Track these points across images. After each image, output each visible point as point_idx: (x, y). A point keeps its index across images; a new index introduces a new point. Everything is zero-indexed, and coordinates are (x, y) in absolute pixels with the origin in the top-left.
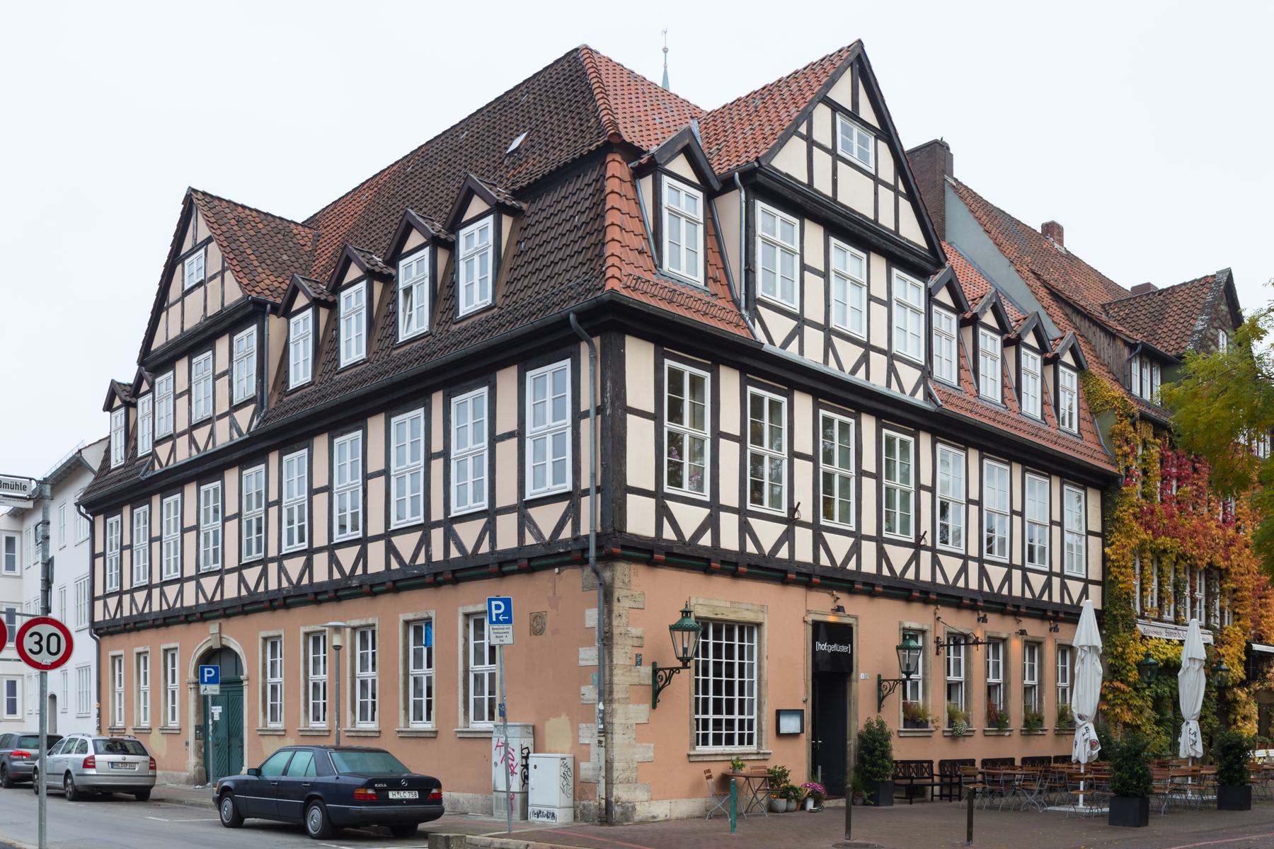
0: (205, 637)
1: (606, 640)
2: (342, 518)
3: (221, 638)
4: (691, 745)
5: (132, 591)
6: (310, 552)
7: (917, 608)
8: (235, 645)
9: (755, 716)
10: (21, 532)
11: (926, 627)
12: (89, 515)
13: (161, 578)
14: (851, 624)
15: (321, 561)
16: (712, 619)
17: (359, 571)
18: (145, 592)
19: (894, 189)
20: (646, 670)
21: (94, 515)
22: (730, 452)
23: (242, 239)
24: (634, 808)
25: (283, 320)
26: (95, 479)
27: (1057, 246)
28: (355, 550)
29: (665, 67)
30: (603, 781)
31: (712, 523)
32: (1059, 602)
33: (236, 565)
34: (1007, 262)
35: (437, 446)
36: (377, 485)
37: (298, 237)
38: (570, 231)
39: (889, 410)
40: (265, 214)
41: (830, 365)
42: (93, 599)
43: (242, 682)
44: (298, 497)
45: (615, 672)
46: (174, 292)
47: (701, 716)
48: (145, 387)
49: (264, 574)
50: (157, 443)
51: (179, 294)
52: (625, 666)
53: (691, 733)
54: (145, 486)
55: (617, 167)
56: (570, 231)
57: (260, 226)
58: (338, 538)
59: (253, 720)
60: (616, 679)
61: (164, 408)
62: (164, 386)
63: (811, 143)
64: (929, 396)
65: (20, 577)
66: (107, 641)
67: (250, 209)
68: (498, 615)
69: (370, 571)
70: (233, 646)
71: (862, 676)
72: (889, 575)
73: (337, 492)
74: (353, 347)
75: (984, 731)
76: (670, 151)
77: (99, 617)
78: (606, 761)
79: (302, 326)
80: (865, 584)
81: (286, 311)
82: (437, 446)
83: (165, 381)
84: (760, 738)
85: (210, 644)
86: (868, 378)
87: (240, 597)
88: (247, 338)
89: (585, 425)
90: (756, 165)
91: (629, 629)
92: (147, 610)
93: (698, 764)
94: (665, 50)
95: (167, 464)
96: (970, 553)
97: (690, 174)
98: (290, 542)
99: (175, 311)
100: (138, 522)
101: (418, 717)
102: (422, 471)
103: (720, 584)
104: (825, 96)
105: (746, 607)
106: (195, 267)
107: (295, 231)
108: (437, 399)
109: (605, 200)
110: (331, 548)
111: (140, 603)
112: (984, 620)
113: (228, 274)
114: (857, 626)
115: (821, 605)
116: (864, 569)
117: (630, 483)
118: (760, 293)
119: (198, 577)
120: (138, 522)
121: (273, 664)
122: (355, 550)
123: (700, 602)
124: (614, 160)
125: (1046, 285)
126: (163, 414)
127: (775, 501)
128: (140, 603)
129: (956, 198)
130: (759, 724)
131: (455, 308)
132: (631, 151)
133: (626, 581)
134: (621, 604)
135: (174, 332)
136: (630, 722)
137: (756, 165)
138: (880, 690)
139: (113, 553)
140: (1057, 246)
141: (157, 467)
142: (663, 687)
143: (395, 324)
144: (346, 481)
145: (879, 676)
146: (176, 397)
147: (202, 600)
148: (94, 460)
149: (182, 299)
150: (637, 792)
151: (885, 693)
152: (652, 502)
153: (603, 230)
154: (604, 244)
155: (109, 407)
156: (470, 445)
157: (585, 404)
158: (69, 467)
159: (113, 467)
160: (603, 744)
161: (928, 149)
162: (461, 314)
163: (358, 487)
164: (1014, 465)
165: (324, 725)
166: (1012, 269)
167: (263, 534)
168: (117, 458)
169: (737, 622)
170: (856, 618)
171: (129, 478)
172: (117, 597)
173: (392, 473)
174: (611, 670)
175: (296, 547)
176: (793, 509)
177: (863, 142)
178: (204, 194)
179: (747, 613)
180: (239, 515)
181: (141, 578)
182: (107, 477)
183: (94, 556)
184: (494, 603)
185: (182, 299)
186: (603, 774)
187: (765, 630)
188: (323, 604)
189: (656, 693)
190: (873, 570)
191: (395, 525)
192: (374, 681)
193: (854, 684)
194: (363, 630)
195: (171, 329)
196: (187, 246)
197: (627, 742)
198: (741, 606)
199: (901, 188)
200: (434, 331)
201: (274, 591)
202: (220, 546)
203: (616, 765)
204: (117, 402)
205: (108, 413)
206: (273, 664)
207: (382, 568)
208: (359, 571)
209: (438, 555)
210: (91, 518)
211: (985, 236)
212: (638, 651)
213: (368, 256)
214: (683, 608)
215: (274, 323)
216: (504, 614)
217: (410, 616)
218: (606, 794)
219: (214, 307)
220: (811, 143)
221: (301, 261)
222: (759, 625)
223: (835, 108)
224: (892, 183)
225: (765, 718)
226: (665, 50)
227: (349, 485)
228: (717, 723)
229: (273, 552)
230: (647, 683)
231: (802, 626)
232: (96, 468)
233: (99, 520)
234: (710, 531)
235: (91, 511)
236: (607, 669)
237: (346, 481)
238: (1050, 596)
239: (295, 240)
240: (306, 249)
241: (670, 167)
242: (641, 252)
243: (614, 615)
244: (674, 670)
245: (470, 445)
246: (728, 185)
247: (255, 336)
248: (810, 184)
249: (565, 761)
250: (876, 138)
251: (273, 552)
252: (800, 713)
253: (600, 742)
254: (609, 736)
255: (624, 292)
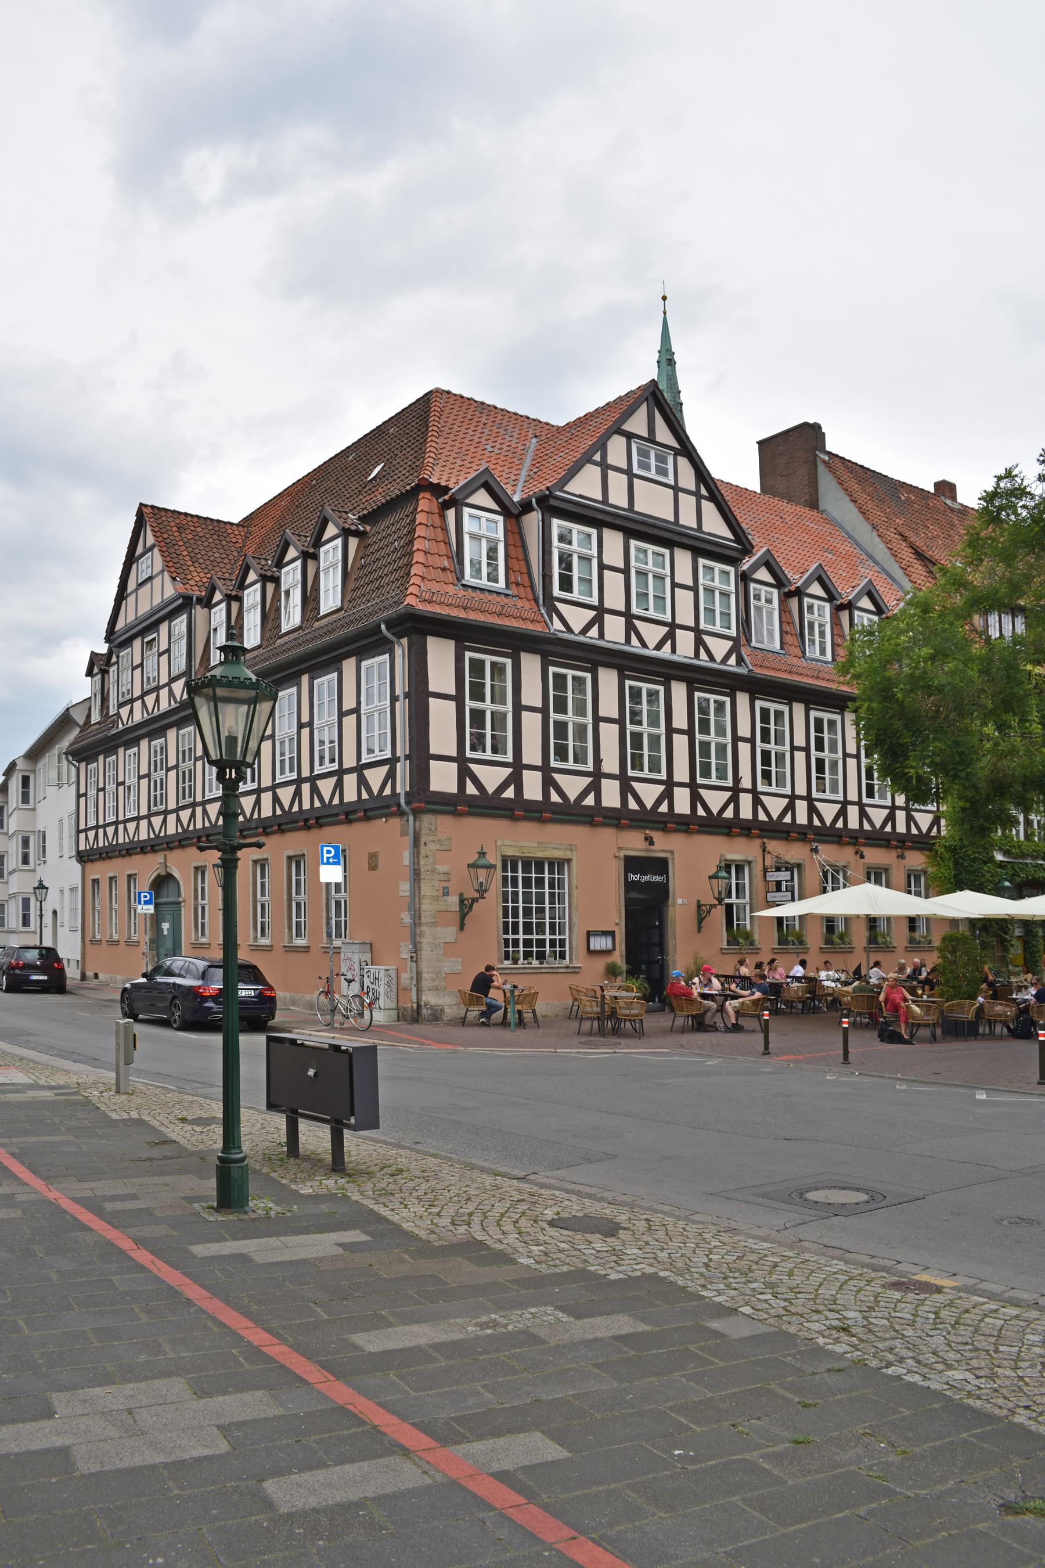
0: (148, 867)
1: (416, 875)
2: (322, 752)
3: (166, 866)
4: (499, 960)
5: (105, 826)
6: (340, 773)
7: (741, 842)
8: (176, 874)
9: (567, 936)
10: (34, 771)
11: (750, 858)
12: (75, 762)
13: (86, 825)
14: (667, 858)
15: (350, 781)
16: (520, 857)
17: (256, 816)
18: (254, 797)
19: (697, 494)
20: (453, 901)
21: (79, 762)
22: (680, 742)
23: (180, 543)
24: (442, 1010)
25: (206, 610)
26: (80, 732)
27: (949, 502)
28: (333, 780)
29: (665, 313)
30: (414, 989)
31: (843, 813)
32: (905, 832)
33: (270, 784)
34: (870, 528)
35: (305, 718)
36: (350, 721)
37: (231, 536)
38: (393, 552)
39: (698, 676)
40: (204, 519)
41: (632, 644)
42: (79, 832)
43: (180, 903)
44: (378, 704)
45: (423, 901)
46: (131, 585)
47: (510, 936)
48: (114, 659)
49: (298, 793)
50: (120, 705)
51: (134, 587)
52: (433, 897)
53: (499, 950)
54: (112, 741)
55: (425, 502)
56: (393, 552)
57: (198, 529)
58: (365, 759)
59: (188, 936)
60: (423, 907)
61: (126, 677)
62: (252, 596)
63: (605, 467)
64: (740, 661)
65: (34, 809)
66: (89, 866)
67: (192, 516)
68: (328, 858)
69: (263, 816)
70: (174, 874)
71: (680, 901)
72: (705, 814)
73: (365, 714)
74: (292, 616)
75: (821, 948)
76: (470, 489)
77: (82, 848)
78: (417, 973)
79: (219, 614)
80: (898, 841)
81: (207, 603)
82: (305, 718)
83: (291, 571)
84: (571, 954)
85: (158, 871)
86: (674, 650)
87: (149, 839)
88: (180, 624)
89: (398, 705)
90: (547, 493)
91: (436, 867)
92: (191, 828)
93: (519, 976)
94: (664, 298)
95: (181, 698)
96: (797, 792)
97: (492, 504)
98: (282, 772)
99: (131, 600)
100: (130, 762)
101: (338, 935)
102: (389, 710)
103: (528, 828)
104: (619, 428)
105: (552, 846)
106: (144, 566)
107: (230, 531)
108: (305, 679)
109: (415, 529)
110: (360, 769)
111: (185, 820)
112: (815, 851)
113: (166, 573)
114: (673, 859)
115: (634, 843)
116: (678, 810)
117: (433, 751)
118: (556, 592)
119: (149, 816)
120: (130, 762)
121: (298, 882)
122: (333, 780)
123: (507, 844)
124: (424, 498)
125: (911, 546)
126: (124, 682)
127: (655, 767)
128: (185, 820)
129: (826, 470)
130: (570, 942)
131: (317, 608)
132: (439, 490)
133: (433, 828)
134: (427, 848)
135: (131, 617)
136: (438, 941)
137: (547, 493)
138: (699, 914)
139: (92, 792)
140: (949, 502)
141: (120, 725)
142: (468, 912)
143: (279, 618)
144: (325, 717)
145: (698, 901)
146: (134, 669)
147: (152, 836)
148: (79, 718)
149: (136, 590)
150: (446, 997)
151: (704, 915)
152: (454, 766)
153: (411, 554)
154: (411, 566)
155: (89, 673)
156: (376, 703)
157: (399, 691)
158: (62, 722)
159: (93, 722)
160: (414, 959)
161: (799, 430)
162: (322, 614)
163: (386, 708)
164: (795, 705)
165: (304, 942)
166: (875, 534)
167: (192, 783)
168: (95, 718)
169: (547, 859)
170: (672, 852)
171: (99, 733)
172: (162, 817)
173: (362, 712)
174: (420, 900)
175: (287, 777)
176: (737, 779)
177: (661, 459)
178: (153, 507)
179: (555, 851)
180: (176, 767)
181: (159, 804)
182: (88, 731)
183: (79, 796)
184: (325, 849)
185: (136, 590)
186: (414, 982)
187: (574, 864)
188: (354, 824)
189: (463, 917)
190: (687, 811)
191: (366, 759)
192: (345, 901)
193: (671, 909)
194: (263, 862)
195: (128, 616)
196: (140, 550)
197: (436, 957)
198: (549, 845)
199: (704, 492)
200: (304, 625)
201: (199, 829)
202: (164, 791)
203: (425, 975)
204: (96, 670)
205: (89, 678)
206: (298, 882)
207: (355, 798)
208: (256, 816)
209: (306, 806)
210: (77, 764)
211: (851, 505)
212: (446, 884)
213: (344, 515)
214: (479, 849)
215: (199, 612)
216: (333, 857)
217: (291, 853)
218: (417, 999)
219: (157, 601)
220: (605, 467)
221: (231, 557)
222: (569, 861)
223: (629, 436)
224: (693, 488)
225: (575, 938)
226: (664, 298)
227: (327, 722)
228: (528, 943)
229: (306, 773)
230: (454, 910)
231: (614, 861)
232: (81, 723)
233: (83, 765)
234: (512, 786)
235: (76, 758)
236: (417, 899)
237: (325, 717)
238: (894, 827)
239: (228, 539)
240: (237, 545)
241: (470, 500)
242: (444, 569)
243: (421, 857)
244: (474, 900)
245: (376, 703)
246: (526, 507)
247: (185, 624)
248: (605, 501)
249: (389, 972)
250: (675, 456)
251: (199, 799)
252: (612, 934)
253: (412, 957)
254: (419, 952)
255: (421, 607)
